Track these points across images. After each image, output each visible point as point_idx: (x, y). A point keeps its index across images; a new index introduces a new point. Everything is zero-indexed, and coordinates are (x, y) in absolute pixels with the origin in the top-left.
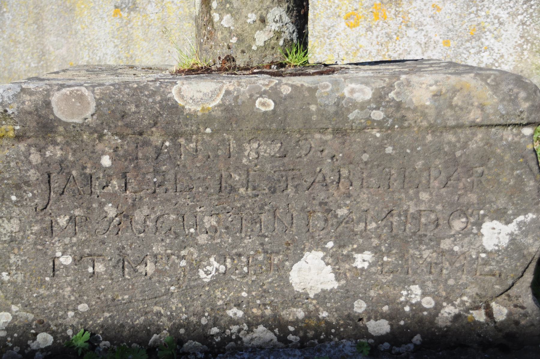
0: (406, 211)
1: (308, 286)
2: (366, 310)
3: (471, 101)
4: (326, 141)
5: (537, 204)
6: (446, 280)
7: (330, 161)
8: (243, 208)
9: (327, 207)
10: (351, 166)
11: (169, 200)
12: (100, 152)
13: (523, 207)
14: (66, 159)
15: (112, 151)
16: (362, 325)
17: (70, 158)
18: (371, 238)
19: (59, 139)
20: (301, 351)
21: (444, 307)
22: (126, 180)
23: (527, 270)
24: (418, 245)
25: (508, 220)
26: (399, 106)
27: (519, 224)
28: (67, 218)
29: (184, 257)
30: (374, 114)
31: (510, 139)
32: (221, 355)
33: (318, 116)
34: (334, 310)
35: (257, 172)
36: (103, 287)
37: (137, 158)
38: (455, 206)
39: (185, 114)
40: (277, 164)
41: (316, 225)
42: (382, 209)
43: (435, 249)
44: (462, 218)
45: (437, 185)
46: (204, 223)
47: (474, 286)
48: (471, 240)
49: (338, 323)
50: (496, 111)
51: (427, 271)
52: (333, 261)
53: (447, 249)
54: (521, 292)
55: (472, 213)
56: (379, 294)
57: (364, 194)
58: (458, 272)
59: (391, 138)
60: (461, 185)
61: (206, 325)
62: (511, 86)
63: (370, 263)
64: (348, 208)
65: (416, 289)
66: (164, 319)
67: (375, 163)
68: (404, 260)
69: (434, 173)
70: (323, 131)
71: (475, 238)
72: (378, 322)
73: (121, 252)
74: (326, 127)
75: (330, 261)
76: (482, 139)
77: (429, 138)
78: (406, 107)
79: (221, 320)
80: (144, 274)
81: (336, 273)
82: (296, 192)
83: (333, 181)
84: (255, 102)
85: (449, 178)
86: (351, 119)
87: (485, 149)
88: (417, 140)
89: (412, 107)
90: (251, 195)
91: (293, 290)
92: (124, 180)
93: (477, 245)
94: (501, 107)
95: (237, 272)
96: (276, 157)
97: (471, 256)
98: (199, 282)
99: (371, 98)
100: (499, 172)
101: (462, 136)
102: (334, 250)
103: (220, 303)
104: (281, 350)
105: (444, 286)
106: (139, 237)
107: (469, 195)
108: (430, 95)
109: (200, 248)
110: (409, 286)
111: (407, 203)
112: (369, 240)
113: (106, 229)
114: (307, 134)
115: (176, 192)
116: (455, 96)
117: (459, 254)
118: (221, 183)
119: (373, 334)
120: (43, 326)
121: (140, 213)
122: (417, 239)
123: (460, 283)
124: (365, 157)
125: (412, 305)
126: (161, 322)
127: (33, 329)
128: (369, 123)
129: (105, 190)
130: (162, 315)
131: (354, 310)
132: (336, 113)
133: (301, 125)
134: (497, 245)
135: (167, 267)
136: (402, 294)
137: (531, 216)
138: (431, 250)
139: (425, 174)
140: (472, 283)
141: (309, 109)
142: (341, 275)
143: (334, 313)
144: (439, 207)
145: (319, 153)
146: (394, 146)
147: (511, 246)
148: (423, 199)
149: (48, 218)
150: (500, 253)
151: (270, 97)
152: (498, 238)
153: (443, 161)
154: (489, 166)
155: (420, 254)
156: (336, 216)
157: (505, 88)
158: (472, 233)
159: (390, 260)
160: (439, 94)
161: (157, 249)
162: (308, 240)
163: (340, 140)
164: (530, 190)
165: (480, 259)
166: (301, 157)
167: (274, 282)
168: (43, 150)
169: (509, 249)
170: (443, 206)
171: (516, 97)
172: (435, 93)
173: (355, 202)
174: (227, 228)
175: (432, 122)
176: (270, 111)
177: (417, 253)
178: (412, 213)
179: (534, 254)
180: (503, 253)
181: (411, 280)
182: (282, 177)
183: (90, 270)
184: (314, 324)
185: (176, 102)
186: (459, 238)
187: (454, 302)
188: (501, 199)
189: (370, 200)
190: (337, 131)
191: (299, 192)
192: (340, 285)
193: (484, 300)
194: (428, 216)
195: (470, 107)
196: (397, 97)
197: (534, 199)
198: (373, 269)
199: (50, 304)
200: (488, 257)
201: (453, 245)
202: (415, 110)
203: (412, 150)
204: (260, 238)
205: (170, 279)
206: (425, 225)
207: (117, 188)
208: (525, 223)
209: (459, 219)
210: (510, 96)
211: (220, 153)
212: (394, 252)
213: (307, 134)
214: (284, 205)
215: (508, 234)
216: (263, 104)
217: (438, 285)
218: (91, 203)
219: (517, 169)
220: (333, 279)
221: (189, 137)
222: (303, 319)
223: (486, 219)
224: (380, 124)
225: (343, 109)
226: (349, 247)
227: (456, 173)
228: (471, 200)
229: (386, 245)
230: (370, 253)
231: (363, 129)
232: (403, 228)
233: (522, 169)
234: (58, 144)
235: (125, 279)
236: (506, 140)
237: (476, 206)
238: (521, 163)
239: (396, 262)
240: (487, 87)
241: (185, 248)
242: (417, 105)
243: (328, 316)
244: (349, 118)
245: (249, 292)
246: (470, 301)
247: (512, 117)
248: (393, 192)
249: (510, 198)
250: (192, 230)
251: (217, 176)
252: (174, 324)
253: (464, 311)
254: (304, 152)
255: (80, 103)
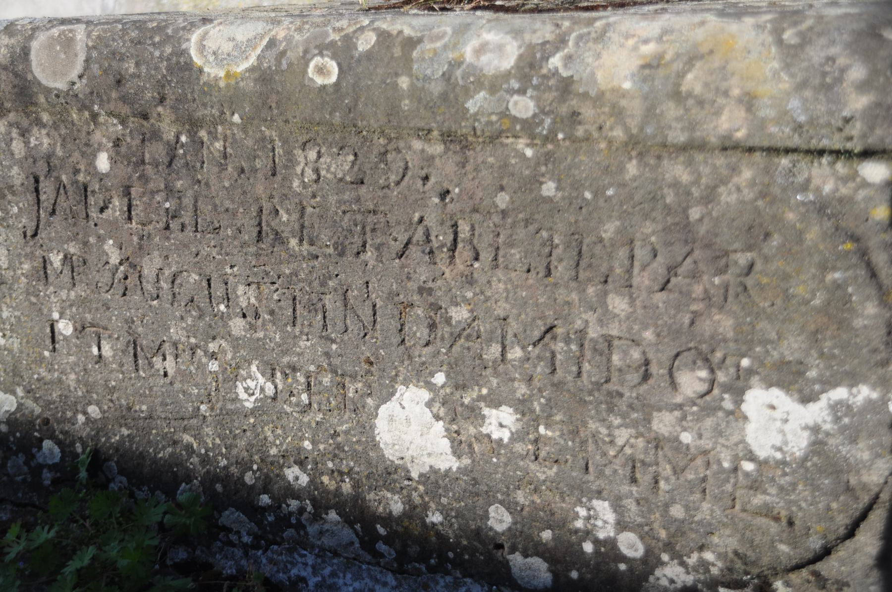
0: (582, 333)
1: (408, 455)
2: (509, 529)
3: (724, 85)
4: (432, 158)
5: (884, 363)
6: (667, 506)
7: (436, 200)
8: (294, 278)
9: (431, 299)
10: (477, 217)
11: (186, 246)
12: (96, 146)
13: (847, 367)
14: (54, 153)
15: (111, 144)
16: (501, 559)
17: (59, 152)
18: (513, 380)
19: (45, 117)
20: (396, 579)
21: (663, 564)
22: (129, 200)
23: (862, 526)
24: (604, 414)
25: (807, 391)
26: (566, 86)
27: (835, 408)
28: (61, 256)
29: (213, 356)
30: (516, 103)
31: (828, 188)
32: (276, 547)
33: (411, 101)
34: (453, 514)
35: (317, 210)
36: (113, 383)
37: (143, 162)
38: (684, 339)
39: (201, 83)
40: (346, 197)
41: (415, 333)
42: (534, 320)
43: (641, 429)
44: (699, 368)
45: (647, 282)
46: (237, 297)
47: (728, 532)
48: (718, 425)
49: (458, 543)
50: (783, 116)
51: (625, 476)
52: (446, 414)
53: (667, 435)
54: (849, 574)
55: (724, 360)
56: (533, 502)
57: (499, 281)
58: (692, 493)
59: (554, 162)
60: (698, 290)
61: (253, 487)
62: (833, 51)
63: (512, 433)
64: (469, 308)
65: (604, 510)
66: (195, 459)
67: (521, 216)
68: (578, 440)
69: (641, 254)
70: (425, 134)
71: (728, 422)
72: (529, 560)
73: (130, 328)
74: (427, 127)
75: (442, 413)
76: (752, 184)
77: (632, 168)
78: (581, 90)
79: (275, 483)
80: (162, 373)
81: (452, 441)
82: (379, 259)
83: (443, 246)
84: (307, 65)
85: (672, 270)
86: (472, 111)
87: (756, 208)
88: (606, 170)
89: (593, 93)
90: (305, 253)
91: (383, 456)
92: (126, 200)
93: (735, 438)
94: (794, 104)
95: (293, 399)
96: (347, 183)
97: (719, 462)
98: (238, 405)
99: (512, 68)
100: (788, 269)
101: (705, 170)
102: (448, 390)
103: (273, 451)
104: (364, 567)
105: (662, 516)
106: (151, 306)
107: (717, 317)
108: (634, 63)
109: (236, 343)
110: (590, 500)
111: (583, 316)
112: (510, 383)
113: (110, 284)
114: (397, 138)
115: (196, 231)
116: (689, 70)
117: (693, 450)
118: (260, 224)
119: (519, 582)
120: (48, 430)
121: (149, 263)
122: (602, 398)
123: (696, 519)
124: (503, 200)
125: (596, 542)
126: (191, 464)
127: (37, 431)
128: (506, 124)
129: (104, 215)
130: (193, 452)
131: (489, 523)
132: (444, 97)
133: (383, 119)
134: (780, 449)
135: (192, 368)
136: (577, 513)
137: (865, 393)
138: (632, 431)
139: (622, 253)
140: (725, 525)
141: (395, 86)
142: (463, 445)
143: (453, 520)
144: (648, 335)
145: (420, 183)
146: (559, 181)
147: (815, 459)
148: (616, 311)
149: (39, 253)
150: (787, 470)
151: (333, 57)
152: (782, 432)
153: (660, 227)
154: (766, 251)
155: (609, 435)
156: (448, 320)
157: (816, 54)
158: (721, 408)
159: (549, 433)
160: (655, 63)
161: (176, 332)
162: (403, 362)
163: (458, 158)
164: (865, 327)
165: (740, 473)
166: (388, 187)
167: (352, 432)
168: (27, 135)
169: (809, 464)
170: (658, 335)
171: (839, 80)
172: (648, 60)
173: (482, 297)
174: (272, 313)
175: (635, 131)
176: (331, 86)
177: (604, 431)
178: (592, 340)
179: (876, 489)
180: (794, 472)
181: (594, 488)
182: (356, 225)
183: (95, 350)
184: (417, 533)
185: (191, 58)
186: (693, 414)
187: (685, 558)
188: (792, 339)
189: (511, 295)
190: (448, 137)
191: (384, 260)
192: (462, 466)
193: (756, 571)
194: (625, 353)
195: (721, 100)
196: (565, 66)
197: (875, 351)
198: (519, 448)
199: (54, 395)
200: (759, 470)
201: (679, 429)
202: (599, 99)
203: (595, 195)
204: (323, 341)
205: (196, 391)
206: (620, 370)
207: (118, 213)
208: (849, 407)
209: (693, 370)
210: (824, 74)
211: (258, 164)
212: (558, 418)
213: (397, 138)
214: (360, 282)
215: (806, 428)
216: (321, 70)
217: (650, 511)
218: (87, 235)
219: (834, 269)
220: (449, 451)
221: (212, 129)
222: (399, 517)
223: (755, 380)
224: (529, 127)
225: (458, 89)
226: (473, 390)
227: (689, 260)
228: (721, 330)
229: (542, 400)
230: (511, 410)
231: (497, 137)
232: (574, 369)
233: (847, 269)
234: (44, 126)
235: (139, 377)
236: (818, 190)
237: (731, 345)
238: (847, 253)
239: (562, 442)
240: (773, 49)
241: (214, 338)
242: (603, 88)
243: (442, 524)
244: (468, 110)
245: (314, 442)
246: (720, 564)
247: (824, 131)
248: (555, 285)
249: (815, 337)
250: (222, 307)
251: (254, 210)
252: (208, 472)
253: (704, 583)
254: (393, 178)
255: (65, 53)
